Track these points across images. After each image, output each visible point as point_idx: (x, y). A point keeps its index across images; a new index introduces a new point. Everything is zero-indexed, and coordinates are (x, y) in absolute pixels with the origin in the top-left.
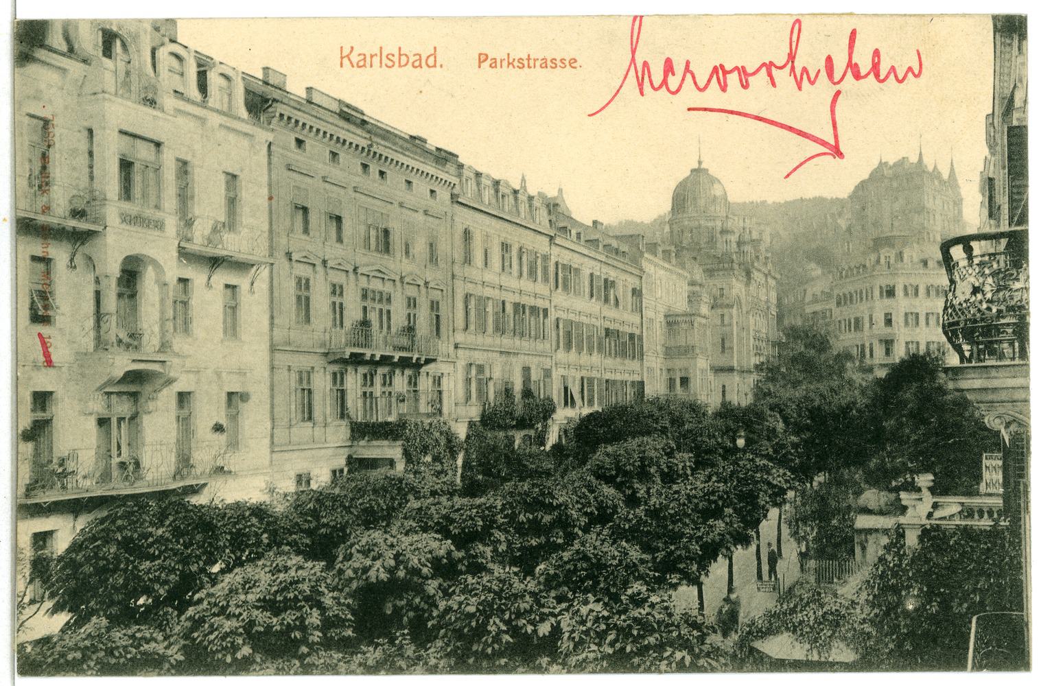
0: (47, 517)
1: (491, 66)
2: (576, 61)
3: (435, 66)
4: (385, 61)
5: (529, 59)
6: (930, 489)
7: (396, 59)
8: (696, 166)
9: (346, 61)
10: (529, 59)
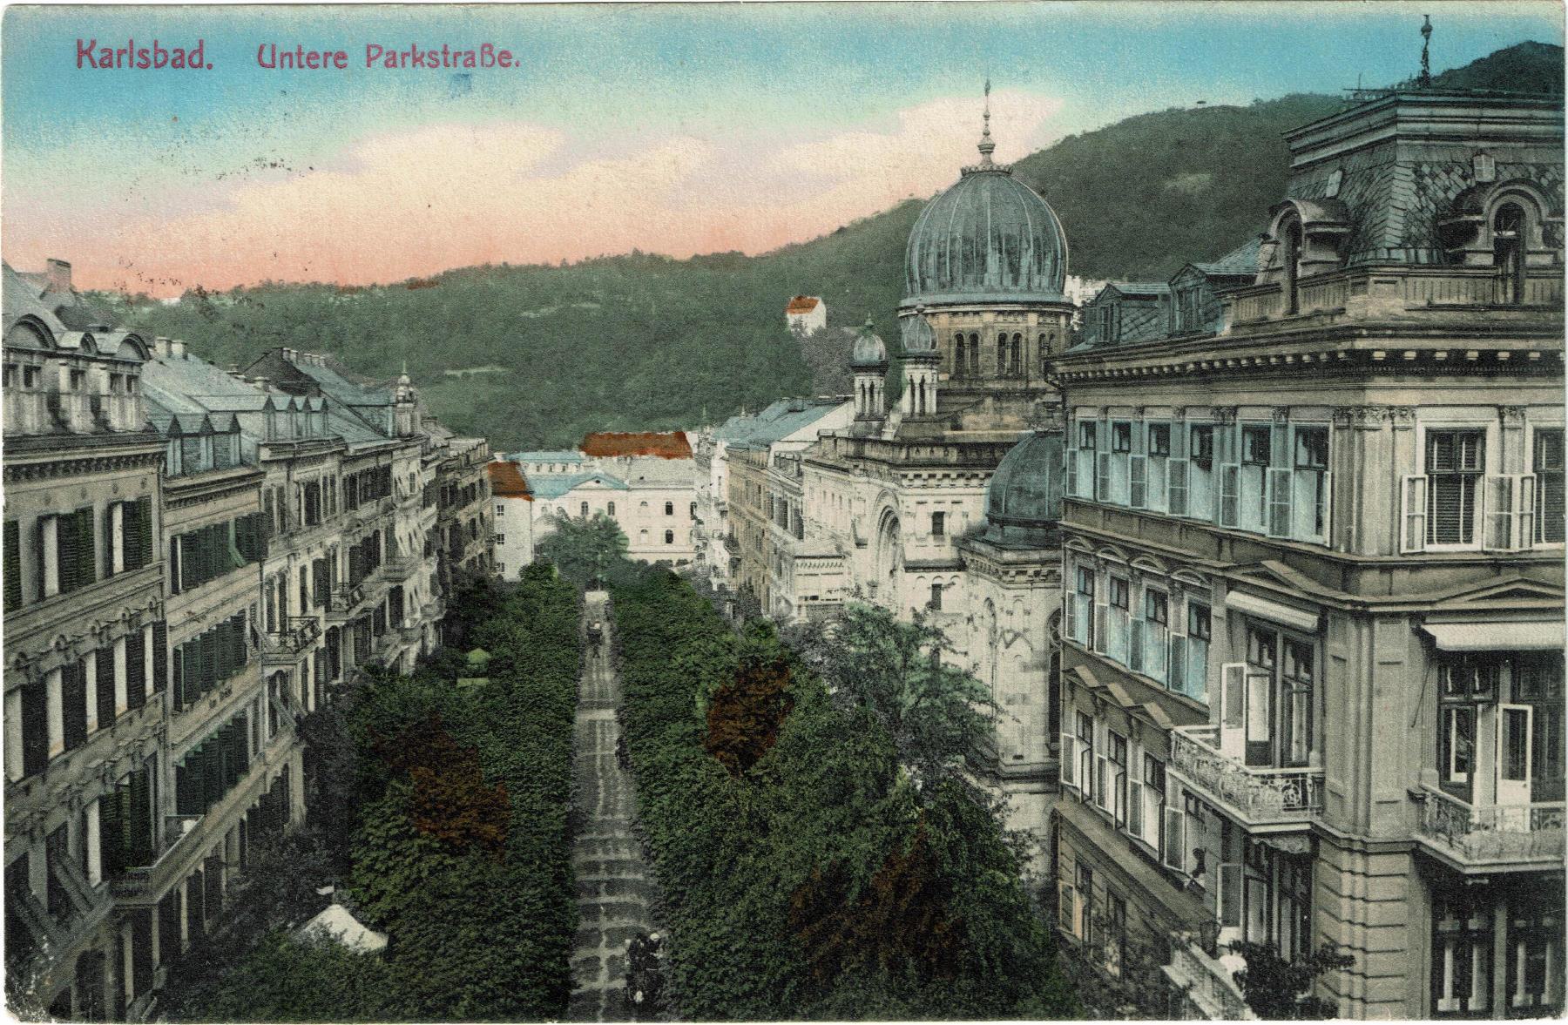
0: (267, 287)
1: (387, 65)
2: (509, 56)
3: (200, 65)
4: (137, 59)
5: (445, 52)
6: (954, 539)
7: (151, 56)
8: (975, 160)
9: (85, 59)
10: (445, 52)
